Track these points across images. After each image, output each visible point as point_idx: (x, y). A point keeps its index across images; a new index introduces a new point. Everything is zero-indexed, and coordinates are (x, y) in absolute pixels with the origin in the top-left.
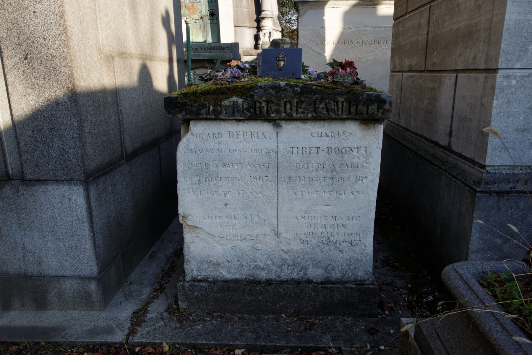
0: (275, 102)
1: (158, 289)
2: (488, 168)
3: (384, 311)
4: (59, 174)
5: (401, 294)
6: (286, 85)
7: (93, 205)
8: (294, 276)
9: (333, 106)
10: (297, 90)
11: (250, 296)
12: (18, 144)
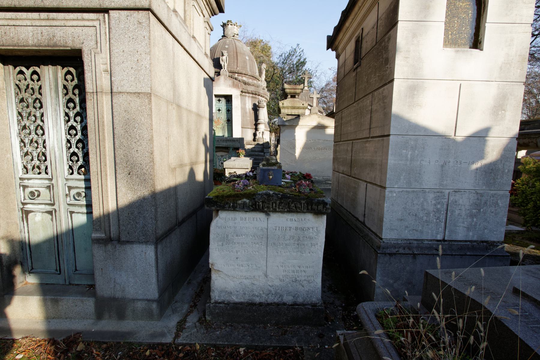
0: (267, 202)
1: (193, 306)
2: (384, 240)
3: (328, 322)
4: (141, 238)
5: (338, 310)
7: (159, 256)
8: (276, 300)
9: (299, 205)
11: (250, 313)
12: (119, 220)
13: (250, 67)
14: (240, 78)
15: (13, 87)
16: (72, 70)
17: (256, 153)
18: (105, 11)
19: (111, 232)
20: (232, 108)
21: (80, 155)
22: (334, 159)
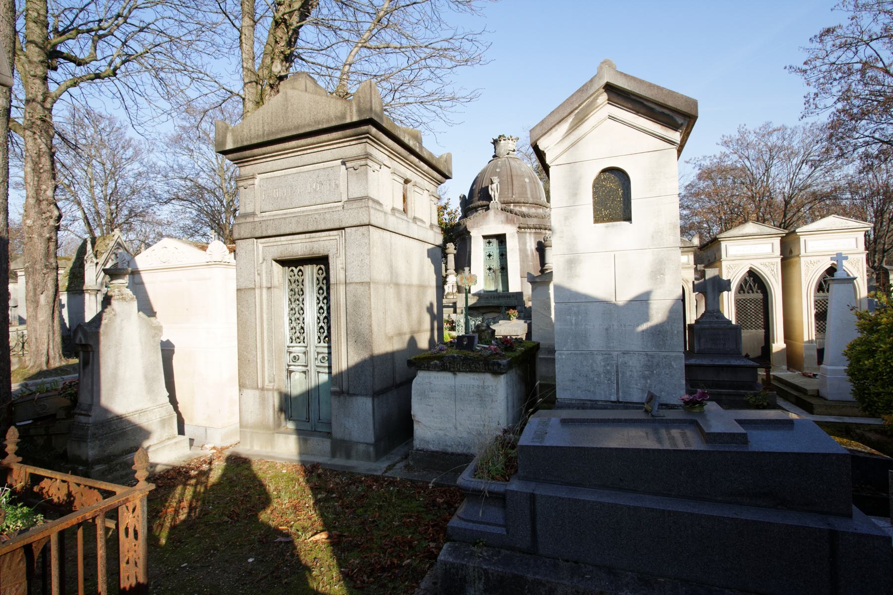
13: (532, 191)
14: (517, 209)
15: (287, 281)
16: (322, 266)
18: (343, 228)
19: (343, 386)
20: (506, 251)
21: (326, 328)
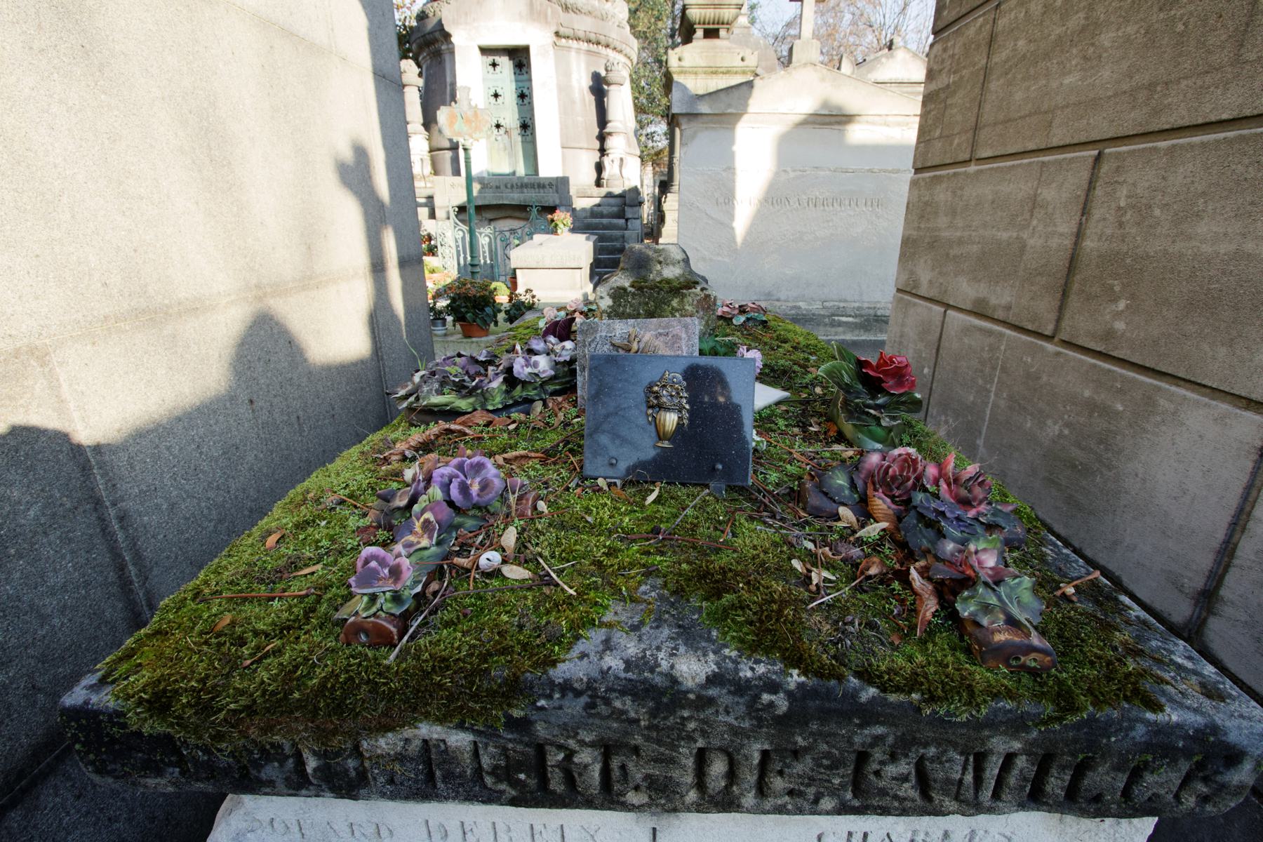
0: (649, 749)
6: (712, 680)
10: (771, 705)
17: (605, 221)
20: (530, 88)
22: (907, 242)
